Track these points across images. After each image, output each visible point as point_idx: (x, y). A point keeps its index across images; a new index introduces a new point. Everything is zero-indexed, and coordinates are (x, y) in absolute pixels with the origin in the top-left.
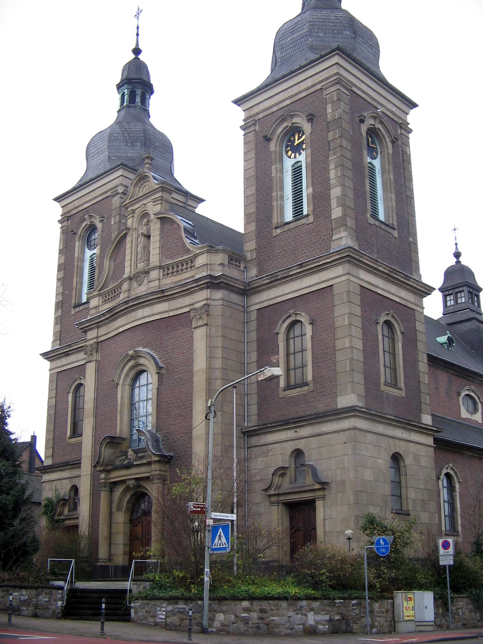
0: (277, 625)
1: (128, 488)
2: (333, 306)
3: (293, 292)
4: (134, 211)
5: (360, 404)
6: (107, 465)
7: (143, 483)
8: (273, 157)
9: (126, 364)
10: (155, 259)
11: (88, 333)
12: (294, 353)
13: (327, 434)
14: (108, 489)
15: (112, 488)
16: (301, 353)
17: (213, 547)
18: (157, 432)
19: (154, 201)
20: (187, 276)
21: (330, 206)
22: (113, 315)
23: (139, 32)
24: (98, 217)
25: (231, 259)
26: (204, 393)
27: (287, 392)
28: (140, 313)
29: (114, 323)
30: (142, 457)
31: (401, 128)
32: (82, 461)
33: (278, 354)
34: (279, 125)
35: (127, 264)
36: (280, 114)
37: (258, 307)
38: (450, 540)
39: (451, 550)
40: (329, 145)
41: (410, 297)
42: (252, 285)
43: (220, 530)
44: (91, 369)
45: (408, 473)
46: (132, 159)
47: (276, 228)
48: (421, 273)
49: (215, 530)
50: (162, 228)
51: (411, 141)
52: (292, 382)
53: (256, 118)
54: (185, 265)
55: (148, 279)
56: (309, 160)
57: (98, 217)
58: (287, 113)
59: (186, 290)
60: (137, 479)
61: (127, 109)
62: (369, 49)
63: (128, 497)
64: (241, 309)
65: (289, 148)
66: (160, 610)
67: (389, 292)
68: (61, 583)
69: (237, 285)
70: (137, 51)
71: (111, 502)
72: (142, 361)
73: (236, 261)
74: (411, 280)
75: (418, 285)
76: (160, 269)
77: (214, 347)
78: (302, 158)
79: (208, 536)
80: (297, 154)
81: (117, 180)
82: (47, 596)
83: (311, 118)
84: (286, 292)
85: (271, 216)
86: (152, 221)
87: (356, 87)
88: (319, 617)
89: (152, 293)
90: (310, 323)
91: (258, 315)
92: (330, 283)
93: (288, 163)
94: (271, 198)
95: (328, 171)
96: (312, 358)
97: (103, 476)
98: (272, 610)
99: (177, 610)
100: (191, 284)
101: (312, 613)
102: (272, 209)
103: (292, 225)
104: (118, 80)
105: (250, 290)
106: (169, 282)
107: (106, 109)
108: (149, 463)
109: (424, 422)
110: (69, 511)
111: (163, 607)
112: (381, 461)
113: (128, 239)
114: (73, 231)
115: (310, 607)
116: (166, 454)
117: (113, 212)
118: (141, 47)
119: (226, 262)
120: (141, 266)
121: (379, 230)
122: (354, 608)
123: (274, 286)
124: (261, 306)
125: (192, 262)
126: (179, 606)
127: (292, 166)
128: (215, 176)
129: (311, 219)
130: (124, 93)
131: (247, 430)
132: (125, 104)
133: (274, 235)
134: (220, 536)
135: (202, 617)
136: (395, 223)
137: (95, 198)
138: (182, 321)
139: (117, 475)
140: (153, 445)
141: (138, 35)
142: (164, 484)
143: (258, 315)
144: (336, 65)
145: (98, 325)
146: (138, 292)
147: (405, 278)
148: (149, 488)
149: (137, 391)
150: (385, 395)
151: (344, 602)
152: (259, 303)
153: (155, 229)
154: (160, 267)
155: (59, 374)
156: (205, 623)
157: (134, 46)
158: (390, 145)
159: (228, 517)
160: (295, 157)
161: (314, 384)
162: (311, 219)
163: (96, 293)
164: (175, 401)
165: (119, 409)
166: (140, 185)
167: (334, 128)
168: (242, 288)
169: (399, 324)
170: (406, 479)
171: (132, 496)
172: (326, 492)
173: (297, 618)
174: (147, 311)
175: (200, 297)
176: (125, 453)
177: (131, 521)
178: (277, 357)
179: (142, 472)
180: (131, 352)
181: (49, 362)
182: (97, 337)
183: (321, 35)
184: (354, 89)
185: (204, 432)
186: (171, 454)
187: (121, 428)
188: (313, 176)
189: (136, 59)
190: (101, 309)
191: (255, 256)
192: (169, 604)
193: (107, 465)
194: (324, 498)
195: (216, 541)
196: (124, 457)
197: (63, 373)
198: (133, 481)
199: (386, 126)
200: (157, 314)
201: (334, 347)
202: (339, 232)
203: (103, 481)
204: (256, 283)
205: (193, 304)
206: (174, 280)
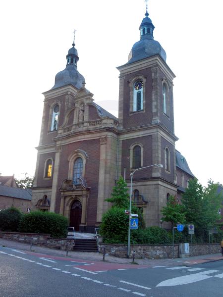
0: (148, 255)
4: (78, 101)
7: (77, 197)
25: (114, 122)
34: (135, 77)
39: (193, 229)
46: (73, 83)
49: (132, 220)
50: (89, 109)
56: (145, 91)
58: (136, 74)
59: (99, 131)
60: (76, 196)
63: (71, 201)
71: (64, 203)
72: (80, 154)
78: (141, 90)
79: (130, 222)
83: (146, 77)
88: (160, 252)
89: (85, 131)
91: (122, 142)
93: (135, 92)
97: (62, 193)
103: (137, 113)
104: (67, 54)
106: (91, 128)
107: (62, 65)
113: (75, 111)
120: (81, 121)
128: (106, 93)
138: (97, 141)
139: (67, 194)
156: (129, 254)
162: (144, 111)
172: (147, 205)
173: (154, 253)
174: (83, 137)
175: (104, 134)
179: (79, 193)
180: (76, 151)
187: (70, 176)
189: (73, 47)
192: (116, 247)
193: (64, 190)
201: (152, 155)
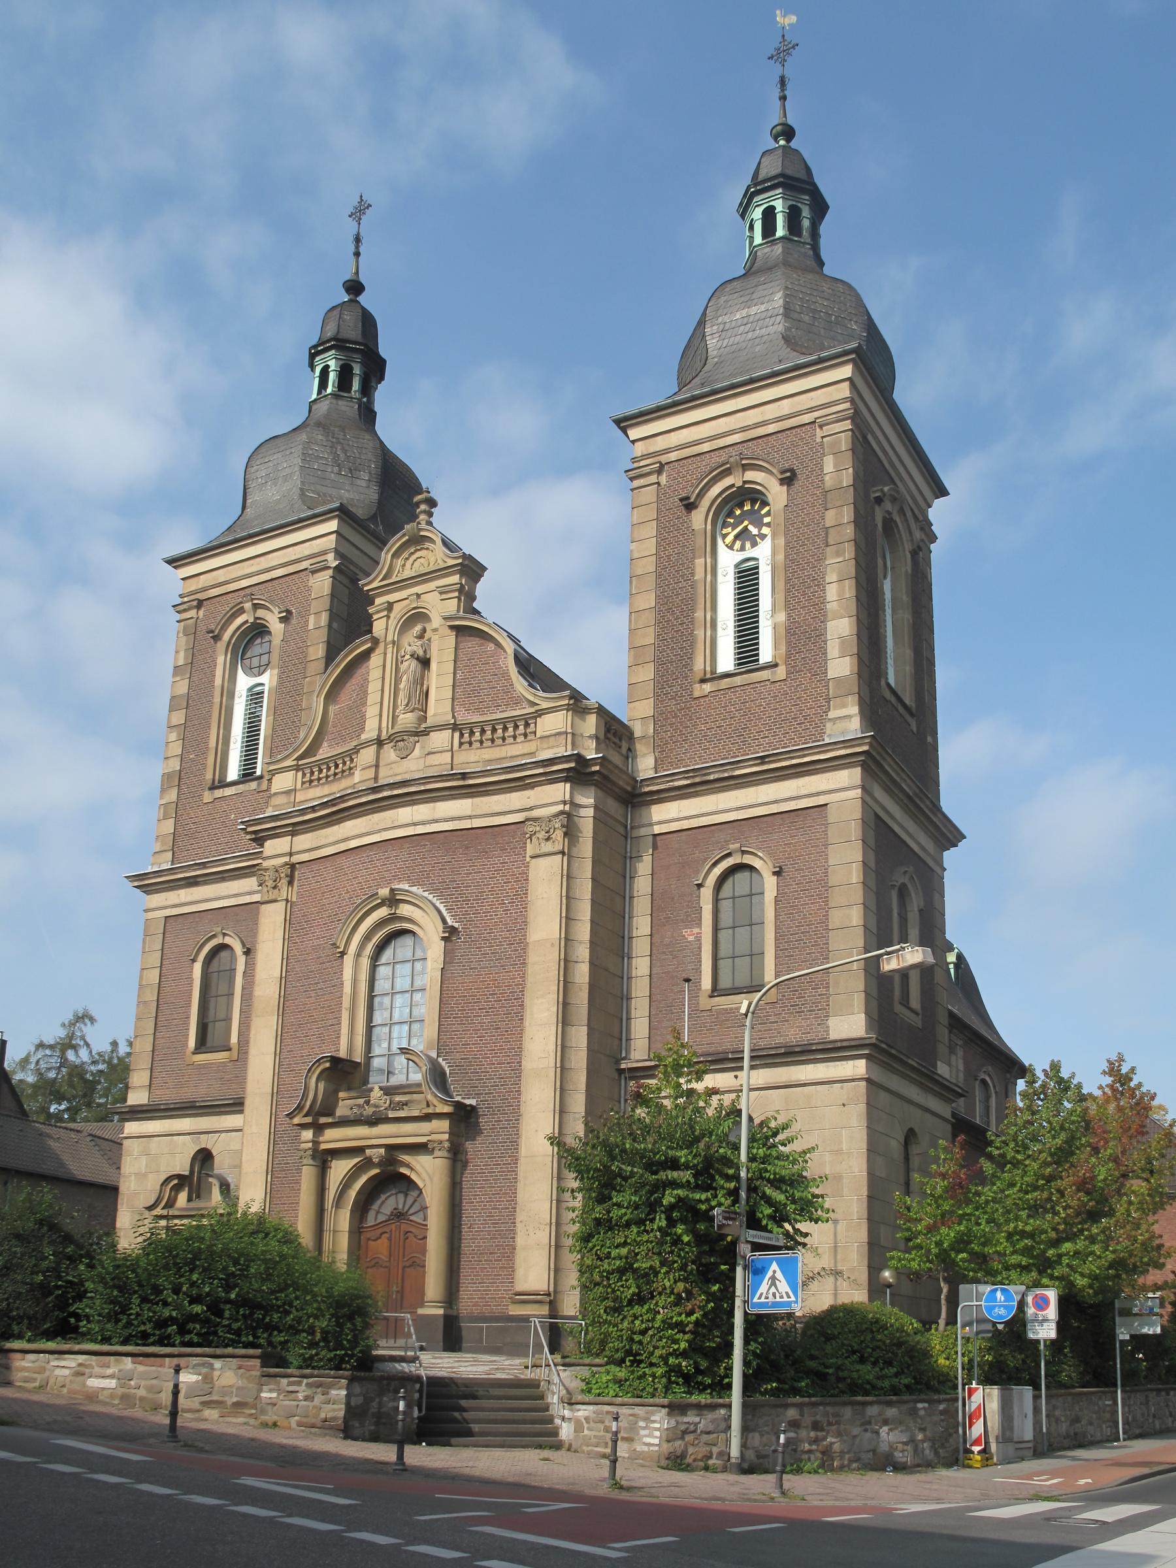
1: (368, 1163)
2: (826, 845)
3: (737, 809)
4: (390, 606)
8: (700, 541)
10: (439, 707)
11: (268, 844)
13: (804, 1085)
16: (730, 931)
17: (755, 1300)
20: (516, 751)
21: (825, 654)
22: (338, 812)
23: (361, 250)
24: (276, 610)
28: (405, 814)
29: (335, 828)
32: (247, 1103)
33: (699, 925)
35: (371, 711)
36: (717, 459)
40: (827, 534)
41: (929, 845)
44: (272, 920)
47: (703, 681)
52: (725, 982)
53: (664, 459)
55: (423, 747)
57: (276, 610)
59: (517, 780)
60: (390, 1148)
61: (334, 401)
64: (622, 830)
66: (644, 1428)
70: (355, 287)
72: (405, 910)
73: (615, 734)
76: (454, 730)
80: (748, 545)
81: (325, 539)
83: (789, 479)
84: (721, 807)
87: (873, 434)
90: (775, 873)
92: (821, 800)
93: (728, 559)
94: (692, 622)
95: (821, 586)
97: (308, 1135)
99: (683, 1427)
100: (530, 769)
101: (886, 1428)
102: (693, 644)
103: (738, 680)
106: (473, 758)
108: (427, 1117)
109: (939, 1072)
110: (190, 1200)
111: (654, 1422)
112: (894, 1143)
114: (212, 632)
117: (314, 603)
120: (407, 719)
125: (527, 725)
126: (686, 1419)
127: (737, 566)
129: (781, 672)
130: (327, 367)
132: (329, 390)
133: (697, 694)
134: (773, 1278)
135: (728, 1441)
138: (507, 838)
145: (296, 830)
146: (400, 770)
153: (442, 647)
154: (455, 727)
155: (171, 920)
160: (742, 549)
162: (781, 672)
163: (289, 762)
164: (479, 997)
166: (405, 555)
174: (422, 811)
178: (696, 930)
182: (291, 854)
183: (806, 319)
184: (869, 437)
186: (473, 1102)
188: (788, 591)
190: (300, 797)
196: (361, 1101)
197: (180, 919)
200: (446, 820)
202: (844, 706)
205: (531, 809)
206: (487, 757)
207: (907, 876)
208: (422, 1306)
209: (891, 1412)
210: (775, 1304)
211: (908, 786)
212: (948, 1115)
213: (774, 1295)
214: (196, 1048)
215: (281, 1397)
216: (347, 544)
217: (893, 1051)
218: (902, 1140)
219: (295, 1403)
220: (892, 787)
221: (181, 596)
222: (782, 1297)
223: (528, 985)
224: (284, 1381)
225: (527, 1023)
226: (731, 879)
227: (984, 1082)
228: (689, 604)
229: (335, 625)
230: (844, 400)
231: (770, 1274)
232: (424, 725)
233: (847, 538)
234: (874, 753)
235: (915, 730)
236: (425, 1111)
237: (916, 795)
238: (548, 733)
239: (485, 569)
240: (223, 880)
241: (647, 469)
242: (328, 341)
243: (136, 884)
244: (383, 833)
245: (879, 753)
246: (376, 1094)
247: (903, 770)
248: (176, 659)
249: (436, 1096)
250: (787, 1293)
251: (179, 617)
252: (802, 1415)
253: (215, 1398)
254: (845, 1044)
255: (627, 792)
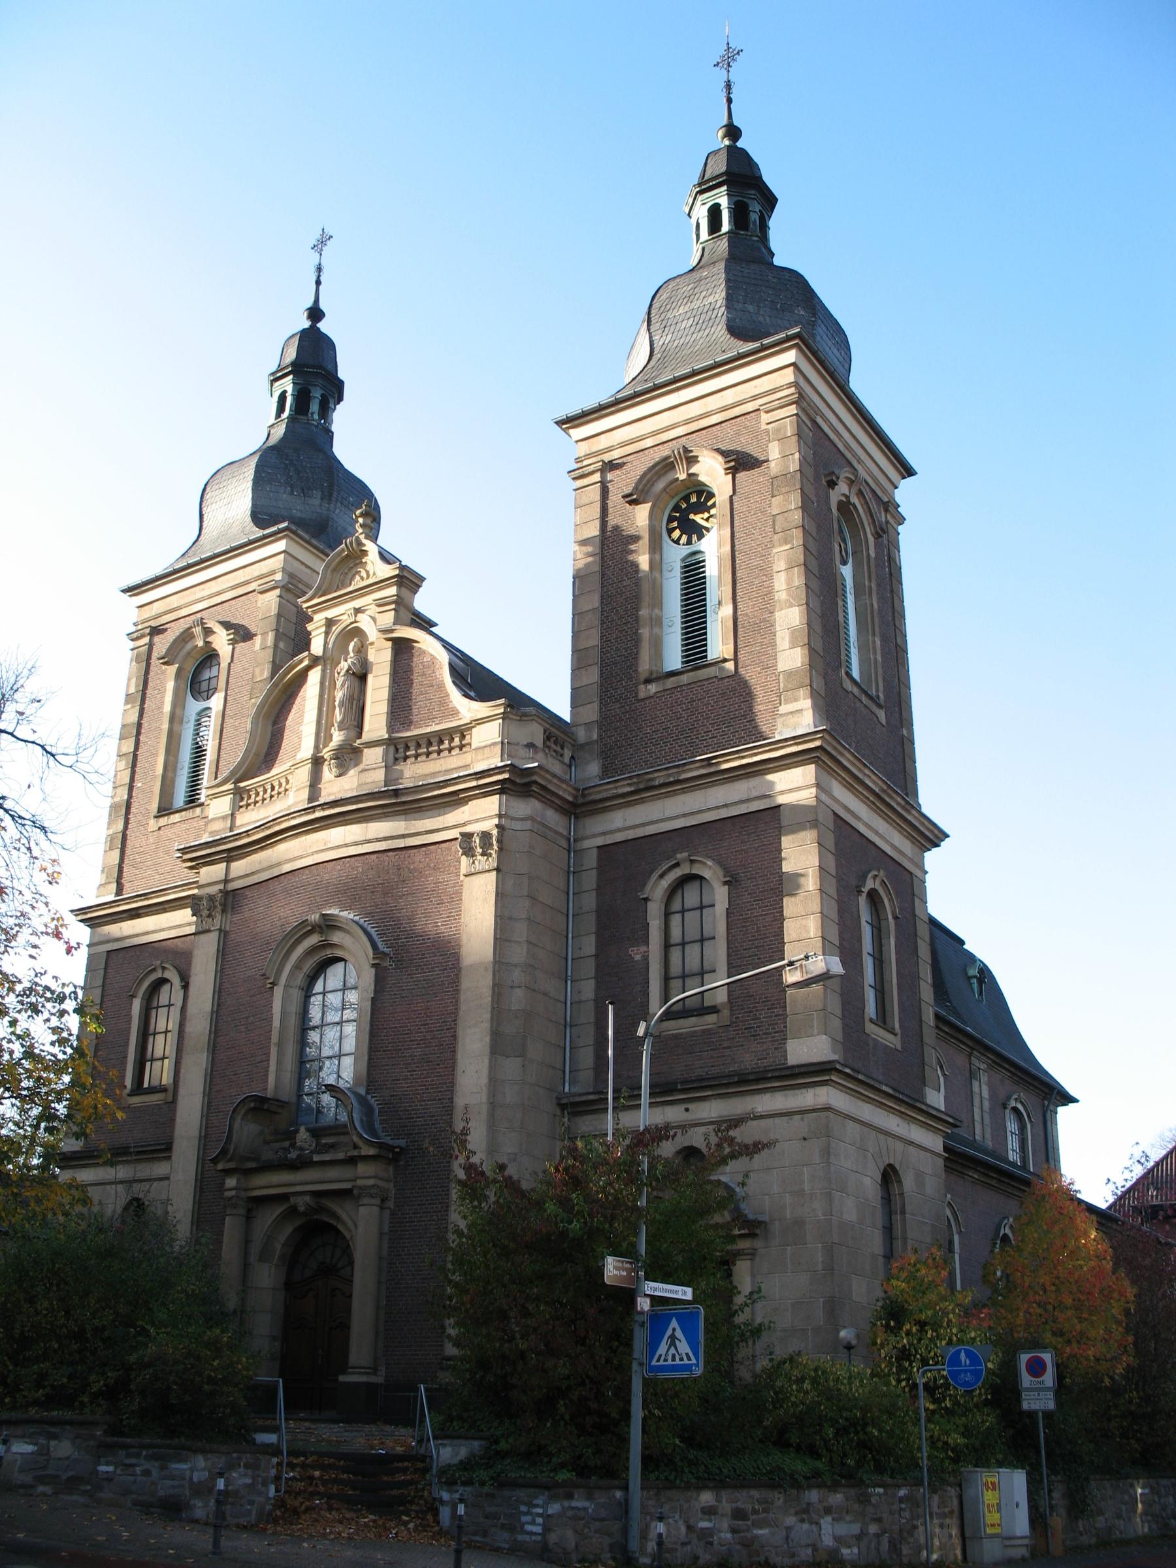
1: (293, 1211)
3: (684, 815)
5: (836, 1057)
6: (248, 1159)
9: (298, 942)
12: (683, 944)
13: (762, 1117)
14: (242, 1212)
15: (249, 1211)
17: (654, 1363)
18: (367, 1093)
19: (381, 603)
23: (322, 279)
25: (548, 737)
26: (488, 1016)
27: (666, 1024)
30: (332, 1146)
31: (886, 510)
32: (175, 1146)
36: (665, 451)
37: (600, 841)
38: (1047, 1357)
39: (1049, 1378)
40: (774, 521)
41: (906, 846)
42: (590, 794)
43: (674, 1323)
45: (908, 1208)
47: (648, 681)
48: (920, 801)
51: (902, 539)
54: (447, 742)
60: (317, 1194)
62: (835, 351)
63: (288, 1230)
65: (675, 524)
67: (877, 833)
68: (271, 1438)
69: (561, 793)
70: (315, 314)
71: (247, 1242)
72: (336, 937)
73: (556, 743)
74: (914, 812)
75: (923, 824)
77: (510, 918)
80: (695, 538)
81: (273, 560)
82: (249, 1472)
85: (636, 657)
86: (372, 644)
88: (843, 1529)
90: (725, 883)
94: (637, 620)
96: (729, 955)
97: (231, 1182)
98: (755, 1512)
99: (570, 1513)
101: (829, 1519)
103: (685, 679)
105: (583, 804)
107: (254, 418)
108: (352, 1161)
111: (537, 1506)
112: (867, 1181)
115: (825, 1504)
116: (388, 1140)
118: (323, 306)
119: (539, 742)
121: (858, 704)
122: (903, 1506)
123: (642, 801)
124: (609, 840)
126: (574, 1504)
127: (683, 560)
131: (572, 1100)
133: (642, 695)
134: (673, 1337)
136: (881, 696)
137: (219, 594)
140: (362, 1120)
141: (318, 283)
142: (382, 1208)
143: (599, 859)
144: (792, 368)
147: (903, 808)
148: (344, 1216)
149: (316, 1001)
150: (871, 1043)
151: (886, 1493)
152: (604, 834)
155: (112, 954)
157: (310, 304)
158: (871, 539)
159: (676, 1292)
160: (689, 542)
161: (731, 1010)
165: (275, 1038)
167: (784, 490)
168: (570, 799)
169: (891, 900)
170: (904, 1220)
171: (295, 1230)
176: (291, 1135)
177: (288, 1286)
178: (644, 949)
179: (334, 1178)
181: (89, 930)
184: (819, 420)
185: (484, 1099)
186: (402, 1143)
187: (276, 1078)
191: (595, 737)
192: (553, 1498)
194: (753, 1254)
195: (662, 1349)
196: (287, 1144)
198: (307, 1198)
199: (867, 503)
202: (796, 700)
203: (233, 1193)
204: (600, 792)
207: (878, 881)
208: (344, 1372)
209: (837, 1498)
210: (674, 1368)
211: (874, 782)
212: (939, 1148)
213: (674, 1356)
214: (132, 1091)
215: (119, 1472)
216: (296, 563)
217: (860, 1077)
218: (879, 1177)
219: (131, 1478)
220: (854, 783)
221: (135, 624)
222: (681, 1359)
223: (461, 1013)
224: (122, 1453)
225: (459, 1056)
226: (680, 892)
227: (1015, 1109)
228: (635, 601)
229: (281, 645)
230: (789, 385)
231: (669, 1332)
232: (358, 741)
233: (794, 524)
234: (829, 749)
235: (884, 721)
236: (349, 1154)
237: (884, 791)
238: (483, 744)
239: (422, 579)
240: (165, 911)
241: (592, 468)
242: (286, 367)
243: (80, 918)
244: (315, 856)
245: (835, 748)
246: (303, 1135)
247: (865, 765)
248: (128, 686)
249: (361, 1137)
250: (687, 1354)
251: (132, 644)
252: (718, 1500)
253: (49, 1472)
254: (803, 1070)
255: (568, 802)
